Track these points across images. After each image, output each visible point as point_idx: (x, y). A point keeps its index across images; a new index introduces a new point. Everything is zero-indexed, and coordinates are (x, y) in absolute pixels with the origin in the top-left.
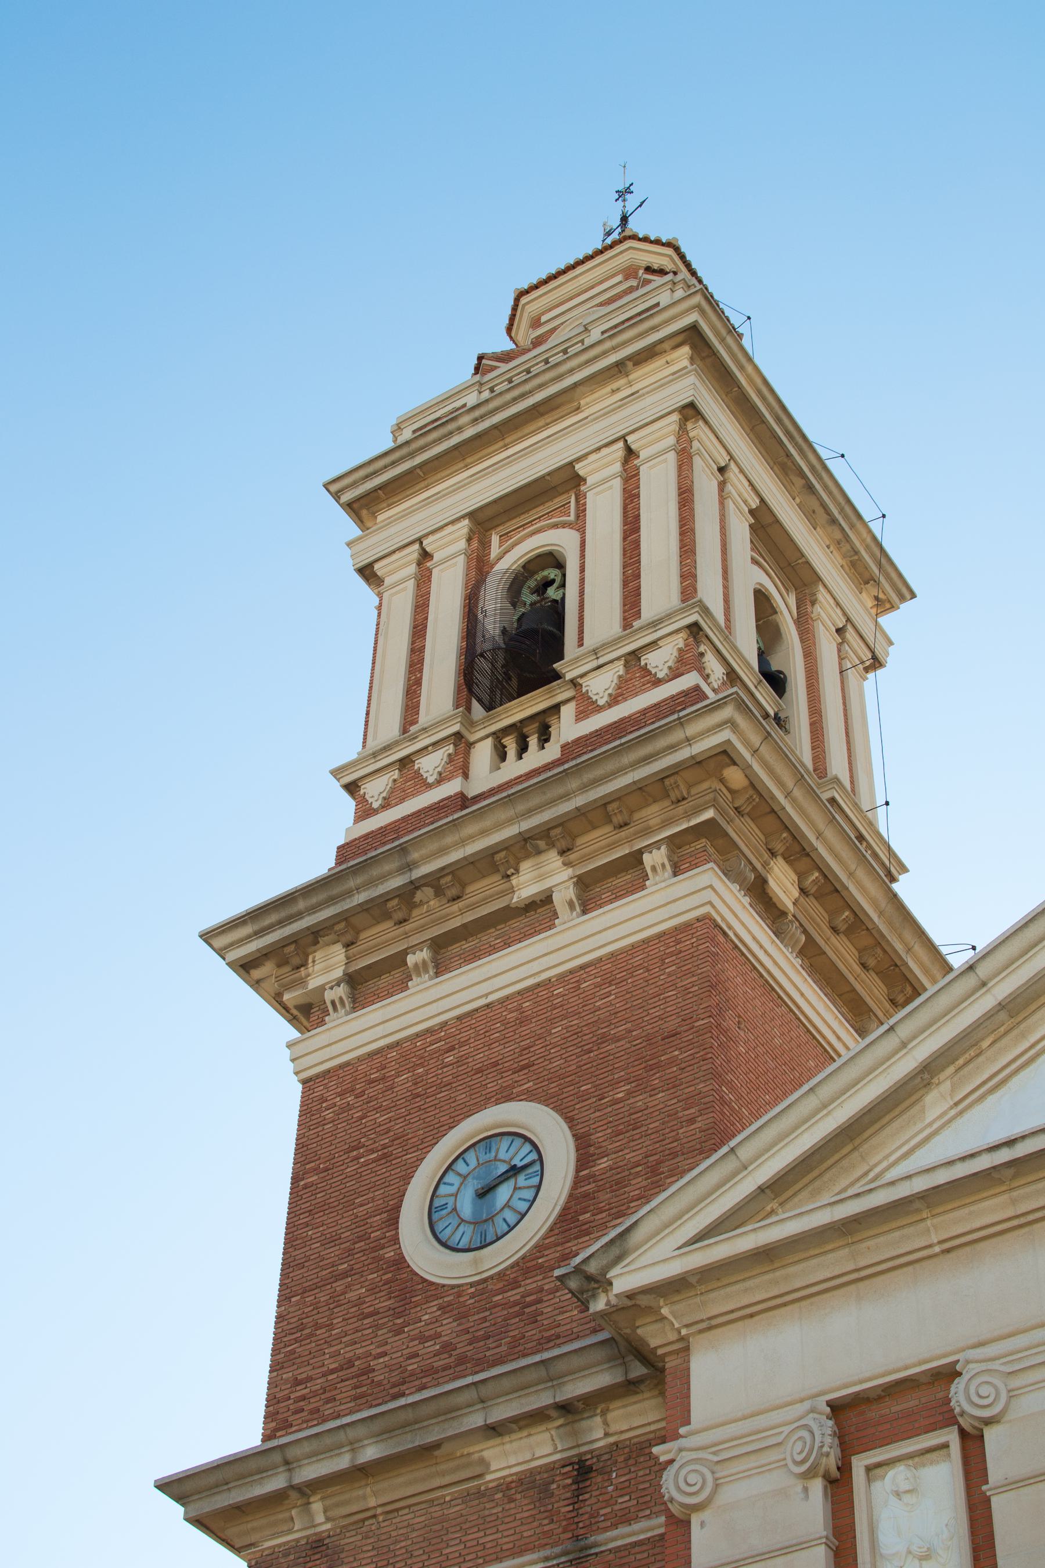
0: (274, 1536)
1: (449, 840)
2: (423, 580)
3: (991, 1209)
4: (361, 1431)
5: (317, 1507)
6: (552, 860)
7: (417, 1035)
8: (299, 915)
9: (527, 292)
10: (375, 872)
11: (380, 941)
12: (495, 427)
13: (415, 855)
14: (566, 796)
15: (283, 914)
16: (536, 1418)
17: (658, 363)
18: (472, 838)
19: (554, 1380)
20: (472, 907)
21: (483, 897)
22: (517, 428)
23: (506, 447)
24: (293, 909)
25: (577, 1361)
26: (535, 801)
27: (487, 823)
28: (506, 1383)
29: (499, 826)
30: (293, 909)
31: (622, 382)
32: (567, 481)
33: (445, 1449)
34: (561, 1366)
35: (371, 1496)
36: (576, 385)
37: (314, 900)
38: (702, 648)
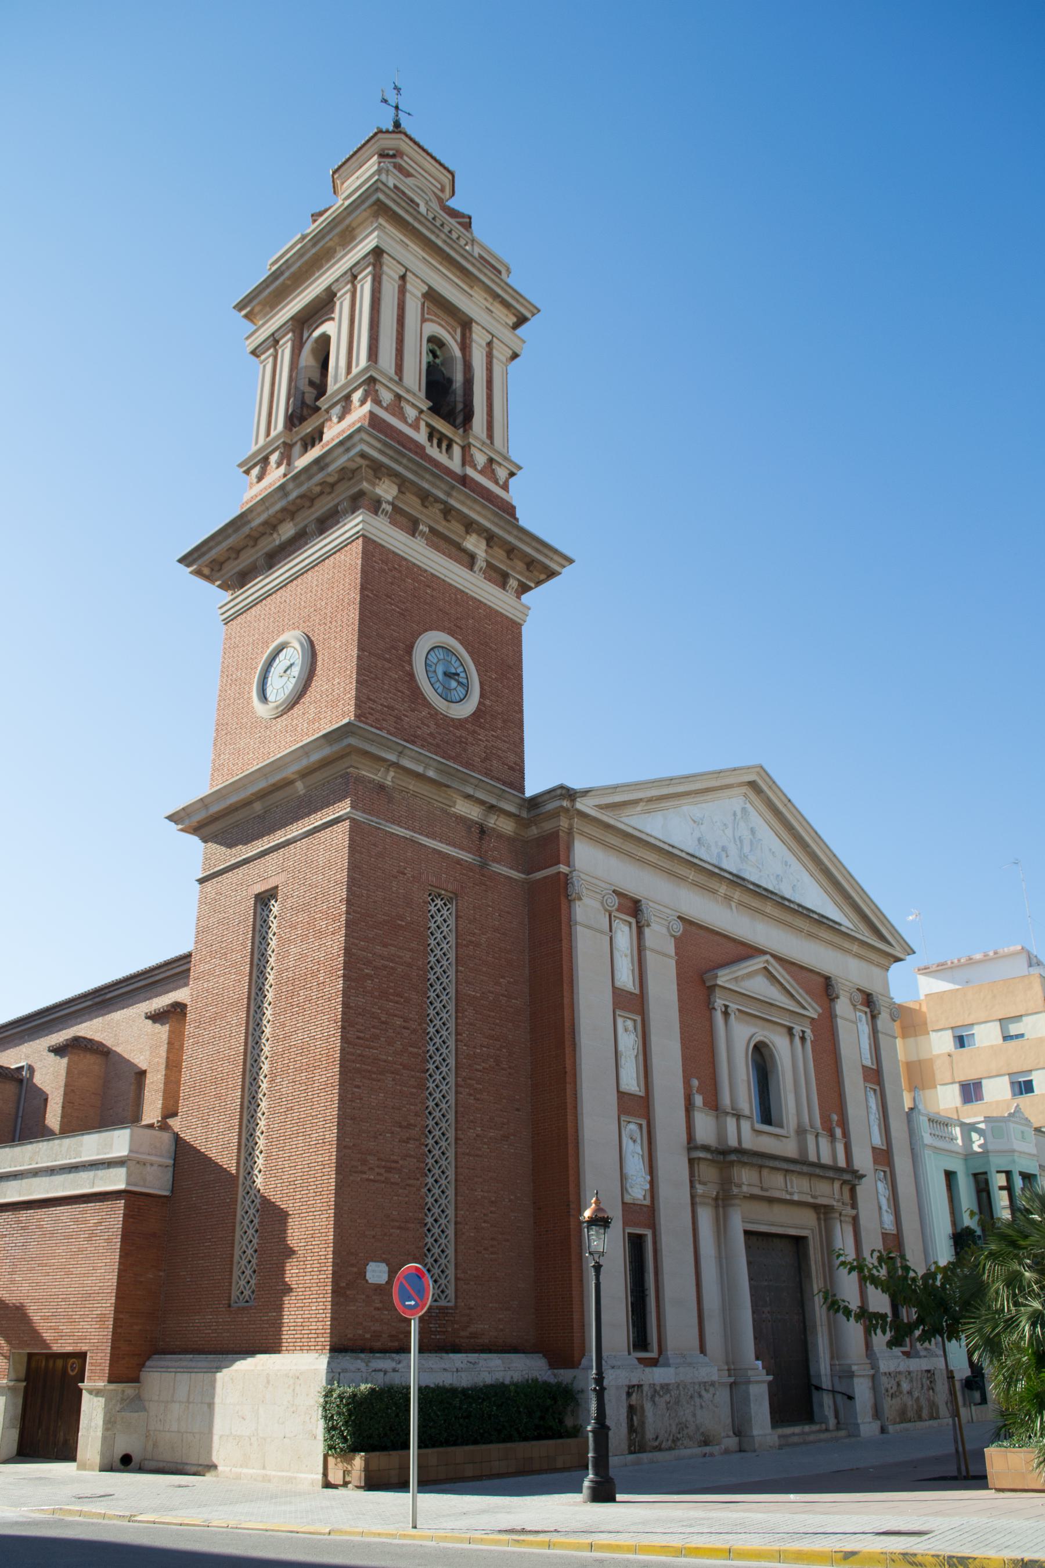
0: (368, 771)
1: (468, 502)
3: (652, 857)
4: (435, 764)
5: (392, 774)
7: (419, 567)
8: (400, 463)
10: (438, 483)
12: (448, 255)
13: (454, 494)
14: (510, 533)
15: (396, 456)
16: (482, 803)
17: (505, 311)
18: (474, 510)
19: (500, 797)
20: (449, 529)
21: (453, 529)
23: (441, 264)
24: (401, 459)
25: (511, 798)
26: (502, 523)
27: (484, 512)
28: (489, 788)
29: (485, 517)
30: (401, 459)
31: (490, 300)
33: (450, 791)
34: (507, 796)
35: (412, 785)
37: (410, 465)
38: (377, 387)
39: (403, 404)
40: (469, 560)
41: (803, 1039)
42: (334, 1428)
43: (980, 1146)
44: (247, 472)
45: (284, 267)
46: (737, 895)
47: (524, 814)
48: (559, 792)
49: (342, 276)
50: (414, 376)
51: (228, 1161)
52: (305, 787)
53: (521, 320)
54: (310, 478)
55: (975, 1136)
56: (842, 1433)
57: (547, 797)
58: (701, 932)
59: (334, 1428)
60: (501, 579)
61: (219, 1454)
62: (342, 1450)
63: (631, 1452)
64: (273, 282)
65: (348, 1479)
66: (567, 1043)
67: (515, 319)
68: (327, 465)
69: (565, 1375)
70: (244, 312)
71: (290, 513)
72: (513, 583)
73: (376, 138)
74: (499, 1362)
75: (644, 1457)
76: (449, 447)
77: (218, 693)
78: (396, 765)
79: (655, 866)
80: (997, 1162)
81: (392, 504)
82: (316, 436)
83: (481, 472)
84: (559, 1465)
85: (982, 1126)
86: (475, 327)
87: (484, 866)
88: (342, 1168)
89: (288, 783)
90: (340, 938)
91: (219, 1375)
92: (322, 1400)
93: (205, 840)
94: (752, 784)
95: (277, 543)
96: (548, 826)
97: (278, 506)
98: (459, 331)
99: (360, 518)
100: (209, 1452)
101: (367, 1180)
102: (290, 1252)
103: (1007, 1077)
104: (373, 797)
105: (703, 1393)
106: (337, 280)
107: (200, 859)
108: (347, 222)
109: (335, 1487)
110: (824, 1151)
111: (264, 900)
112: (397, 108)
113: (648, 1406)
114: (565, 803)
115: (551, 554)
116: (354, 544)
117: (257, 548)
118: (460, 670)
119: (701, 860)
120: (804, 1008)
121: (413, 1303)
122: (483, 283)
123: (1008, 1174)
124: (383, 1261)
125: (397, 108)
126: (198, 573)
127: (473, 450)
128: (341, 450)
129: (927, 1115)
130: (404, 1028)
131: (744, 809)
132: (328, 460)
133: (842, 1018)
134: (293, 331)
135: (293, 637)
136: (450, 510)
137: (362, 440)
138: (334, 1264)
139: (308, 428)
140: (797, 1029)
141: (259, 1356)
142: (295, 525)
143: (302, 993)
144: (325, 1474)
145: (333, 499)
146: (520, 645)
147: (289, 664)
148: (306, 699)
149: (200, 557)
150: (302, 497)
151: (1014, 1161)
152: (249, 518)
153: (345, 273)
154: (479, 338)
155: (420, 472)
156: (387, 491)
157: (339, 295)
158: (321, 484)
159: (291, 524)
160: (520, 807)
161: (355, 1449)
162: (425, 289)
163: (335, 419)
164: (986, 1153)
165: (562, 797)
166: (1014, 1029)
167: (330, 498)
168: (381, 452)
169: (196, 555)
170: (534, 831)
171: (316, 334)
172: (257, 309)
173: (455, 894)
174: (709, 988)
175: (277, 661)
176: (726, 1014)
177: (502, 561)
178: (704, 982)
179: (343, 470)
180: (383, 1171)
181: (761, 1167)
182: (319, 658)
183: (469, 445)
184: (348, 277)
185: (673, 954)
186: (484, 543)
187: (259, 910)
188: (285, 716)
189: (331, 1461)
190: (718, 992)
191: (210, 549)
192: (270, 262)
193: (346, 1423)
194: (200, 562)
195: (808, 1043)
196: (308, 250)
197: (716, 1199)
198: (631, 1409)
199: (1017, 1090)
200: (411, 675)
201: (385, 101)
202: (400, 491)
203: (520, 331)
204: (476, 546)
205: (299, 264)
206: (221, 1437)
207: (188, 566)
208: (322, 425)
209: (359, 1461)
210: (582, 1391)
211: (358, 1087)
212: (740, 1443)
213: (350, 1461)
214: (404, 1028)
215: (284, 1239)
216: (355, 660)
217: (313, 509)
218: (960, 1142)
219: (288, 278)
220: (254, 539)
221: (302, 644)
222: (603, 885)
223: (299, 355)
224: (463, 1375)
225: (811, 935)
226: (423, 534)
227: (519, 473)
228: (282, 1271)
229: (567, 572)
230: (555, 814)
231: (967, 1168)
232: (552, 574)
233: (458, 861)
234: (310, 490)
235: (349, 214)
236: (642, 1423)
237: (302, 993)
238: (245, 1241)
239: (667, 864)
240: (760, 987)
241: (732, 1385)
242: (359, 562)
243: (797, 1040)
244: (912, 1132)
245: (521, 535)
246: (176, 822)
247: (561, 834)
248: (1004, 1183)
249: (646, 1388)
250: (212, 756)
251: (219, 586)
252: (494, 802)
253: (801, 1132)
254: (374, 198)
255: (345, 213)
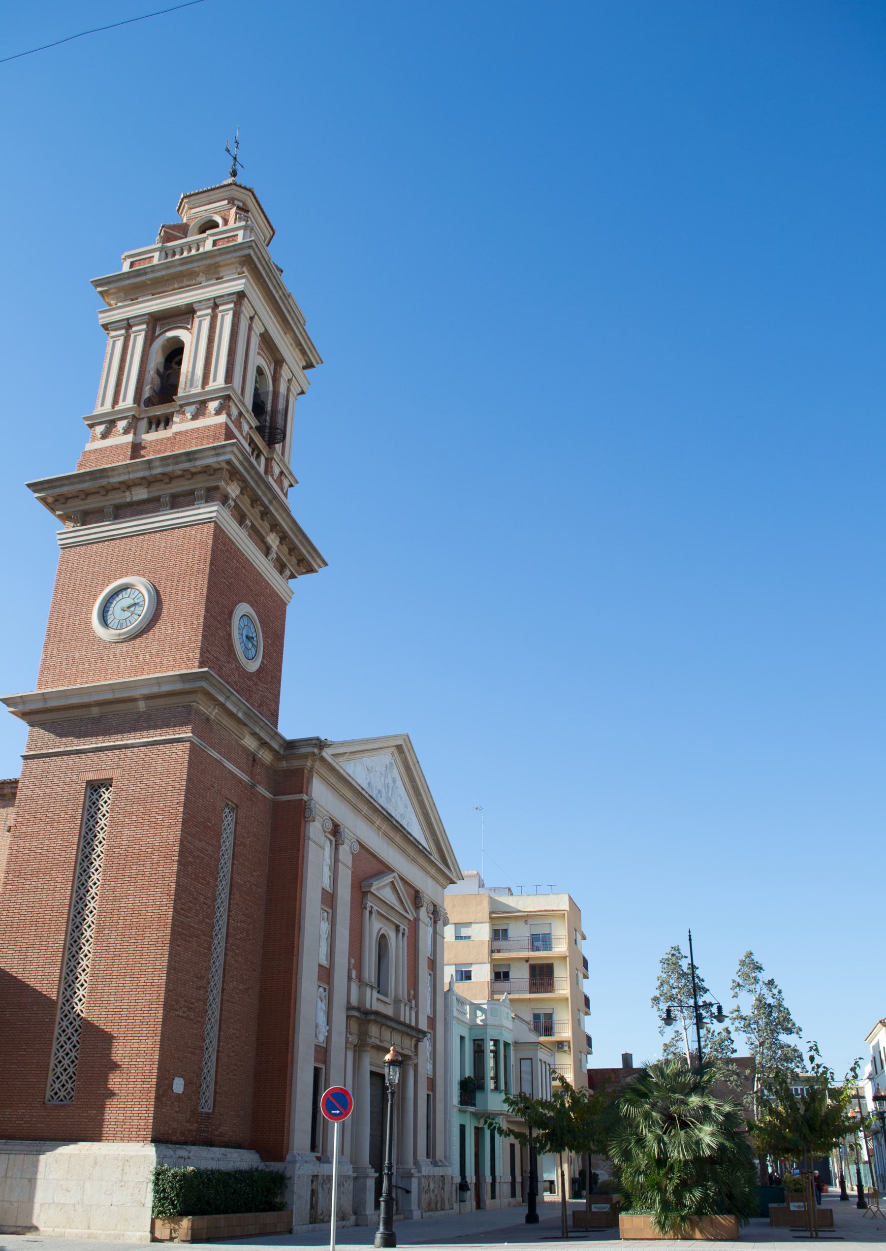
1: (280, 511)
3: (349, 794)
8: (249, 473)
9: (253, 194)
10: (267, 493)
12: (280, 307)
14: (297, 537)
15: (249, 468)
20: (261, 526)
21: (263, 526)
22: (278, 313)
33: (244, 728)
35: (226, 721)
36: (293, 331)
39: (242, 420)
40: (267, 550)
41: (403, 934)
42: (164, 1198)
43: (481, 1021)
44: (91, 426)
45: (149, 270)
46: (384, 827)
47: (282, 752)
48: (314, 742)
49: (205, 300)
50: (249, 400)
51: (50, 988)
52: (146, 706)
53: (309, 366)
54: (177, 463)
55: (479, 1013)
56: (402, 1216)
57: (305, 743)
59: (164, 1198)
60: (281, 567)
61: (38, 1219)
62: (171, 1214)
63: (311, 1223)
64: (134, 277)
65: (174, 1235)
66: (297, 926)
67: (305, 364)
68: (196, 459)
69: (275, 1166)
70: (99, 289)
71: (148, 482)
72: (288, 573)
73: (230, 188)
74: (236, 1155)
75: (317, 1225)
76: (258, 456)
77: (51, 604)
78: (222, 706)
80: (492, 1033)
81: (234, 501)
82: (167, 421)
83: (275, 481)
84: (278, 1230)
85: (485, 1006)
86: (285, 367)
87: (253, 786)
88: (168, 1007)
89: (133, 700)
90: (177, 831)
91: (42, 1157)
92: (153, 1178)
93: (32, 725)
94: (399, 748)
95: (128, 500)
96: (296, 764)
97: (141, 474)
98: (273, 365)
99: (215, 508)
100: (30, 1213)
101: (179, 1016)
102: (115, 1066)
103: (454, 967)
104: (204, 727)
106: (200, 302)
107: (25, 739)
108: (218, 259)
109: (161, 1241)
110: (406, 1016)
111: (95, 787)
112: (235, 159)
113: (320, 1190)
114: (316, 751)
115: (316, 557)
116: (206, 525)
117: (107, 498)
118: (254, 635)
120: (407, 912)
121: (338, 1112)
122: (295, 333)
123: (496, 1042)
124: (182, 1077)
125: (235, 159)
126: (43, 500)
127: (274, 464)
128: (213, 452)
129: (457, 995)
130: (205, 903)
131: (391, 763)
132: (197, 456)
134: (148, 324)
135: (141, 584)
136: (267, 513)
137: (232, 452)
138: (158, 1078)
139: (159, 411)
140: (402, 927)
141: (81, 1145)
142: (149, 492)
143: (134, 867)
144: (152, 1231)
145: (190, 484)
146: (284, 621)
147: (132, 602)
148: (150, 635)
149: (50, 488)
150: (163, 474)
151: (502, 1034)
152: (110, 474)
153: (209, 299)
154: (285, 373)
155: (259, 483)
156: (233, 490)
157: (199, 313)
158: (184, 471)
159: (146, 490)
160: (281, 746)
161: (183, 1213)
162: (262, 330)
163: (189, 416)
164: (485, 1025)
165: (315, 745)
166: (464, 932)
167: (188, 482)
168: (241, 463)
169: (46, 486)
170: (284, 764)
171: (170, 334)
172: (111, 291)
173: (237, 806)
174: (364, 893)
175: (120, 596)
176: (371, 912)
177: (284, 555)
178: (361, 888)
179: (208, 467)
180: (186, 1009)
181: (382, 1025)
182: (165, 606)
183: (272, 458)
184: (211, 303)
185: (350, 866)
186: (278, 540)
187: (89, 793)
188: (126, 644)
189: (158, 1223)
190: (369, 896)
191: (63, 485)
192: (127, 254)
193: (177, 1195)
194: (50, 492)
195: (406, 937)
196: (175, 266)
197: (355, 1046)
199: (459, 977)
200: (229, 635)
201: (228, 150)
202: (242, 493)
203: (307, 371)
204: (273, 541)
205: (164, 273)
206: (42, 1205)
207: (35, 491)
208: (172, 414)
209: (186, 1223)
210: (290, 1178)
211: (179, 946)
212: (356, 1220)
213: (177, 1222)
214: (205, 903)
215: (109, 1055)
216: (202, 619)
217: (169, 486)
218: (468, 1016)
219: (150, 280)
220: (107, 490)
221: (148, 591)
222: (326, 813)
223: (151, 345)
224: (221, 1163)
225: (414, 860)
226: (246, 526)
227: (296, 486)
228: (106, 1081)
229: (322, 571)
230: (305, 756)
231: (470, 1035)
232: (311, 570)
233: (240, 781)
234: (173, 471)
235: (221, 254)
236: (317, 1202)
237: (134, 867)
238: (60, 1054)
239: (355, 800)
240: (388, 895)
241: (355, 1178)
242: (210, 542)
243: (401, 934)
244: (446, 1006)
245: (303, 540)
246: (8, 705)
247: (306, 771)
248: (492, 1048)
249: (320, 1178)
250: (41, 656)
251: (59, 516)
252: (268, 740)
253: (397, 1001)
254: (246, 252)
255: (217, 253)
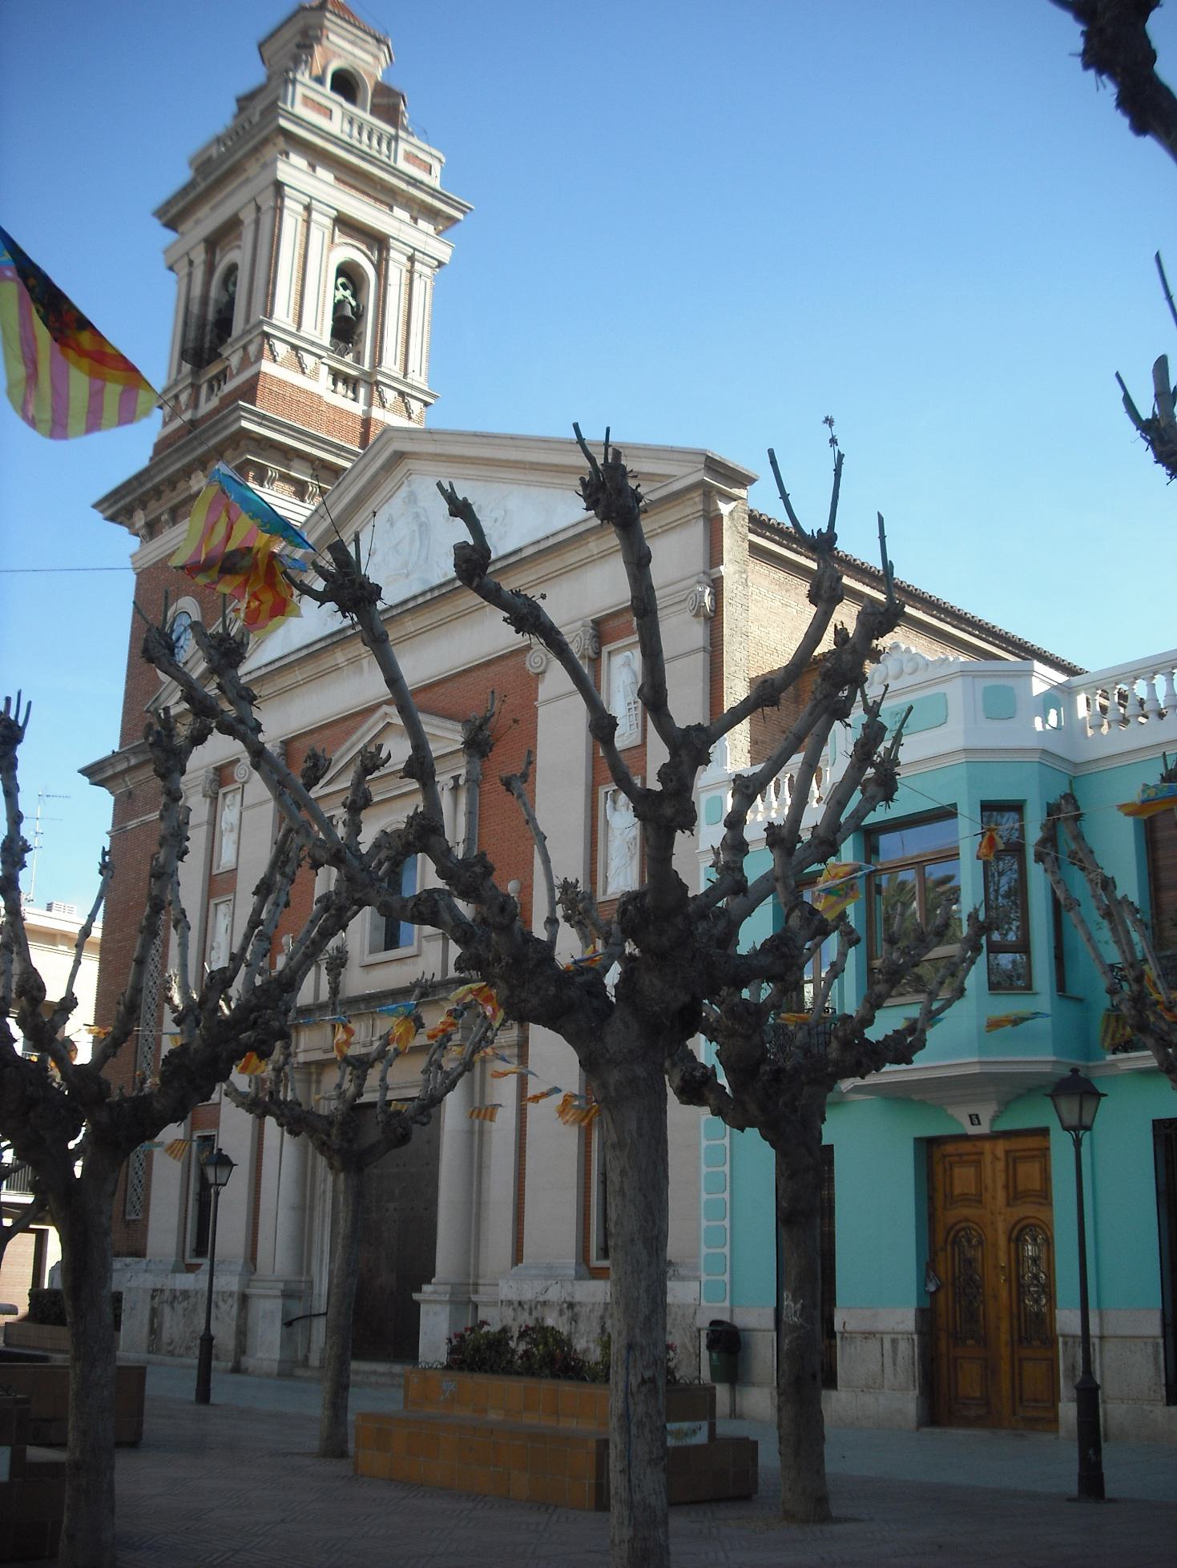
2: (190, 275)
6: (201, 474)
11: (159, 509)
32: (231, 228)
58: (493, 669)
79: (308, 681)
105: (221, 1303)
113: (167, 1309)
119: (564, 530)
133: (570, 694)
198: (154, 1313)
236: (161, 1325)
249: (167, 1293)
